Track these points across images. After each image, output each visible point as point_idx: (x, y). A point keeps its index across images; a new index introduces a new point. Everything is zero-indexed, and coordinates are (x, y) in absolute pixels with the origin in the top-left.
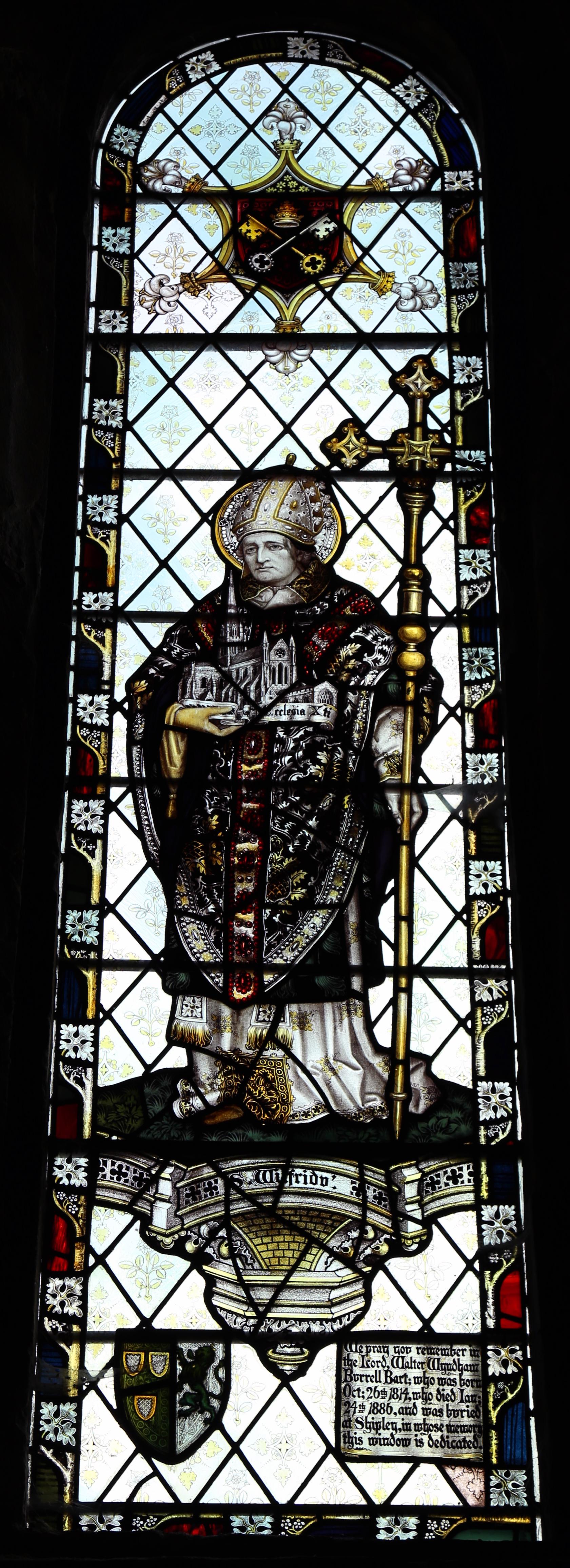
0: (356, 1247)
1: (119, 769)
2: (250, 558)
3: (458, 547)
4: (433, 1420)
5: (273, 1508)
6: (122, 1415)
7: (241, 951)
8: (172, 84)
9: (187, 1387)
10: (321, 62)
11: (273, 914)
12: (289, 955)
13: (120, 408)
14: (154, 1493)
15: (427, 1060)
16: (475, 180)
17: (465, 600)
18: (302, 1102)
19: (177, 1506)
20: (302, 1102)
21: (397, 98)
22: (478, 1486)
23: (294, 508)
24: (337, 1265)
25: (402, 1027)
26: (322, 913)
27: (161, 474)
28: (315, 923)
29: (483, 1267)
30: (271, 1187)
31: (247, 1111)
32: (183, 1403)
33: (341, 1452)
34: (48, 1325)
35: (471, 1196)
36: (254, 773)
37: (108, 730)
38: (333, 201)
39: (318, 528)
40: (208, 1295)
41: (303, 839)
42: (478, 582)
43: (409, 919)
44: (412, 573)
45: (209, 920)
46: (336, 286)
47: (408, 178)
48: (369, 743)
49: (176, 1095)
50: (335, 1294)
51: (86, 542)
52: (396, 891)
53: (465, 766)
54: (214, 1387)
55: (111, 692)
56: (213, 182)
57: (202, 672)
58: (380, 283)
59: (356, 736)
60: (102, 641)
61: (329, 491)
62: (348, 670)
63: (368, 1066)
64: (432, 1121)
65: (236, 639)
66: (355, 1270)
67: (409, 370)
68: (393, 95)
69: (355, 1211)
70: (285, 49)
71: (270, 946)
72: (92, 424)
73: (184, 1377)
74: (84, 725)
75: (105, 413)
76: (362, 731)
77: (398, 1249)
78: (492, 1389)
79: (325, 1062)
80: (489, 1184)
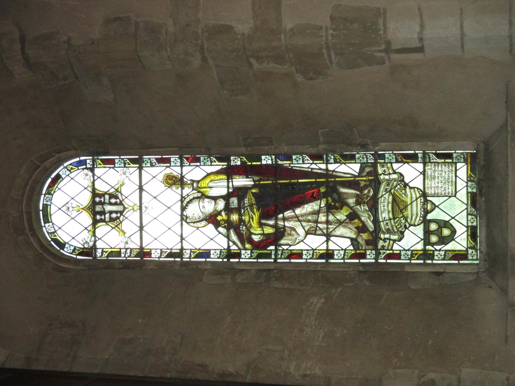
40: (415, 225)
77: (403, 180)
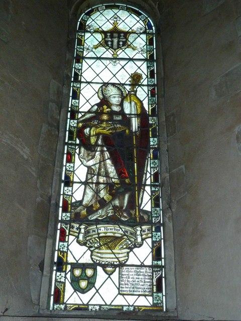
27: (89, 83)
38: (126, 34)
40: (91, 255)
46: (125, 48)
58: (134, 49)
77: (135, 246)
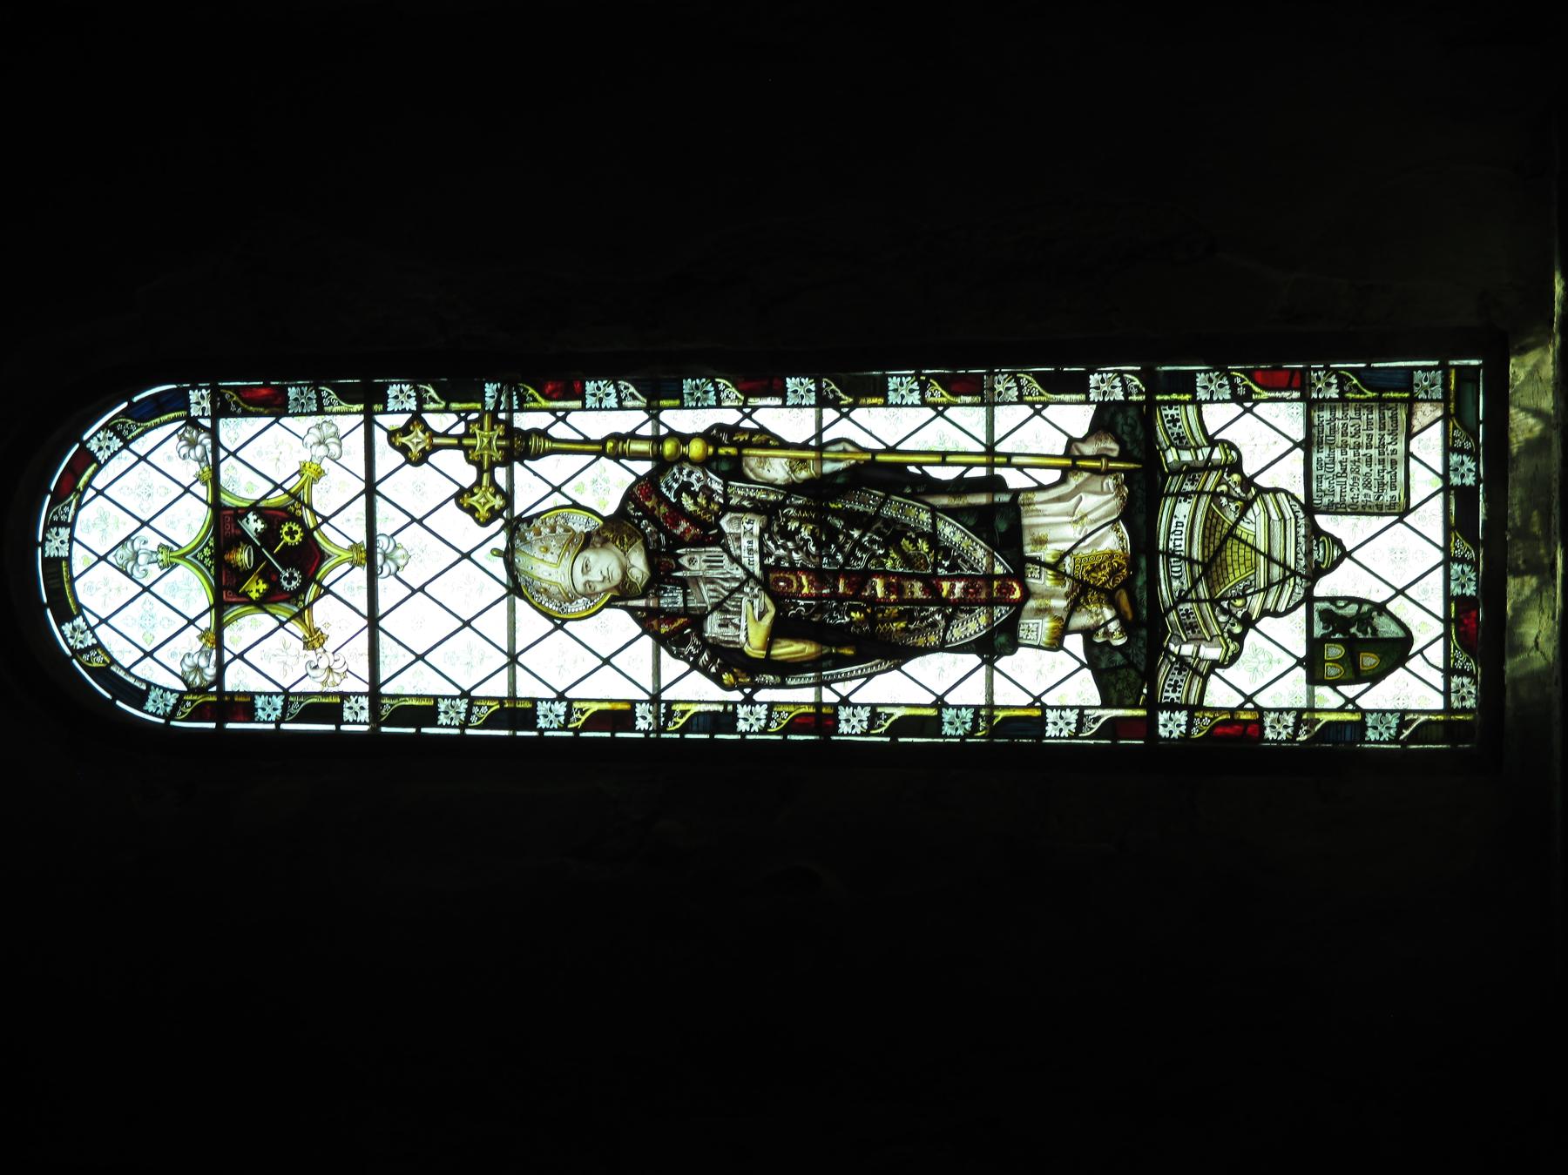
0: (1235, 500)
1: (808, 695)
2: (599, 588)
3: (583, 408)
4: (1375, 441)
5: (1447, 562)
6: (1375, 678)
7: (977, 592)
8: (98, 662)
9: (1353, 630)
10: (72, 526)
11: (942, 566)
12: (980, 553)
13: (447, 702)
14: (1436, 654)
15: (1072, 441)
16: (200, 389)
17: (637, 403)
18: (1112, 542)
19: (1446, 635)
20: (1112, 542)
21: (111, 457)
22: (1427, 407)
23: (547, 550)
24: (1250, 514)
25: (1043, 460)
26: (940, 525)
27: (513, 659)
28: (950, 531)
29: (1250, 400)
30: (1186, 566)
31: (1119, 587)
32: (1365, 632)
33: (1402, 511)
34: (1302, 738)
35: (1190, 408)
36: (810, 583)
37: (771, 706)
39: (567, 530)
41: (872, 541)
42: (618, 392)
43: (944, 454)
44: (613, 448)
45: (949, 619)
46: (315, 513)
47: (199, 449)
48: (779, 487)
49: (1107, 643)
50: (1274, 516)
51: (585, 728)
52: (919, 465)
53: (799, 406)
54: (1352, 610)
55: (734, 704)
56: (206, 622)
57: (713, 627)
59: (772, 497)
60: (684, 713)
61: (529, 520)
62: (708, 503)
63: (1078, 489)
64: (1125, 438)
65: (680, 599)
66: (1254, 499)
67: (404, 449)
68: (107, 461)
69: (1205, 500)
70: (58, 560)
71: (972, 568)
72: (465, 725)
73: (1345, 631)
74: (767, 725)
75: (452, 714)
76: (768, 493)
77: (1236, 467)
78: (1350, 395)
79: (1075, 523)
80: (1179, 393)
